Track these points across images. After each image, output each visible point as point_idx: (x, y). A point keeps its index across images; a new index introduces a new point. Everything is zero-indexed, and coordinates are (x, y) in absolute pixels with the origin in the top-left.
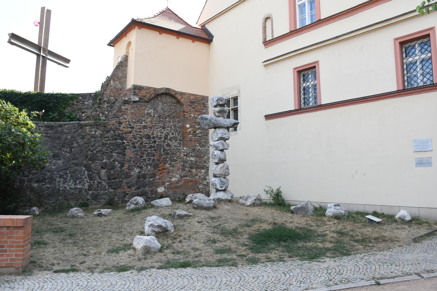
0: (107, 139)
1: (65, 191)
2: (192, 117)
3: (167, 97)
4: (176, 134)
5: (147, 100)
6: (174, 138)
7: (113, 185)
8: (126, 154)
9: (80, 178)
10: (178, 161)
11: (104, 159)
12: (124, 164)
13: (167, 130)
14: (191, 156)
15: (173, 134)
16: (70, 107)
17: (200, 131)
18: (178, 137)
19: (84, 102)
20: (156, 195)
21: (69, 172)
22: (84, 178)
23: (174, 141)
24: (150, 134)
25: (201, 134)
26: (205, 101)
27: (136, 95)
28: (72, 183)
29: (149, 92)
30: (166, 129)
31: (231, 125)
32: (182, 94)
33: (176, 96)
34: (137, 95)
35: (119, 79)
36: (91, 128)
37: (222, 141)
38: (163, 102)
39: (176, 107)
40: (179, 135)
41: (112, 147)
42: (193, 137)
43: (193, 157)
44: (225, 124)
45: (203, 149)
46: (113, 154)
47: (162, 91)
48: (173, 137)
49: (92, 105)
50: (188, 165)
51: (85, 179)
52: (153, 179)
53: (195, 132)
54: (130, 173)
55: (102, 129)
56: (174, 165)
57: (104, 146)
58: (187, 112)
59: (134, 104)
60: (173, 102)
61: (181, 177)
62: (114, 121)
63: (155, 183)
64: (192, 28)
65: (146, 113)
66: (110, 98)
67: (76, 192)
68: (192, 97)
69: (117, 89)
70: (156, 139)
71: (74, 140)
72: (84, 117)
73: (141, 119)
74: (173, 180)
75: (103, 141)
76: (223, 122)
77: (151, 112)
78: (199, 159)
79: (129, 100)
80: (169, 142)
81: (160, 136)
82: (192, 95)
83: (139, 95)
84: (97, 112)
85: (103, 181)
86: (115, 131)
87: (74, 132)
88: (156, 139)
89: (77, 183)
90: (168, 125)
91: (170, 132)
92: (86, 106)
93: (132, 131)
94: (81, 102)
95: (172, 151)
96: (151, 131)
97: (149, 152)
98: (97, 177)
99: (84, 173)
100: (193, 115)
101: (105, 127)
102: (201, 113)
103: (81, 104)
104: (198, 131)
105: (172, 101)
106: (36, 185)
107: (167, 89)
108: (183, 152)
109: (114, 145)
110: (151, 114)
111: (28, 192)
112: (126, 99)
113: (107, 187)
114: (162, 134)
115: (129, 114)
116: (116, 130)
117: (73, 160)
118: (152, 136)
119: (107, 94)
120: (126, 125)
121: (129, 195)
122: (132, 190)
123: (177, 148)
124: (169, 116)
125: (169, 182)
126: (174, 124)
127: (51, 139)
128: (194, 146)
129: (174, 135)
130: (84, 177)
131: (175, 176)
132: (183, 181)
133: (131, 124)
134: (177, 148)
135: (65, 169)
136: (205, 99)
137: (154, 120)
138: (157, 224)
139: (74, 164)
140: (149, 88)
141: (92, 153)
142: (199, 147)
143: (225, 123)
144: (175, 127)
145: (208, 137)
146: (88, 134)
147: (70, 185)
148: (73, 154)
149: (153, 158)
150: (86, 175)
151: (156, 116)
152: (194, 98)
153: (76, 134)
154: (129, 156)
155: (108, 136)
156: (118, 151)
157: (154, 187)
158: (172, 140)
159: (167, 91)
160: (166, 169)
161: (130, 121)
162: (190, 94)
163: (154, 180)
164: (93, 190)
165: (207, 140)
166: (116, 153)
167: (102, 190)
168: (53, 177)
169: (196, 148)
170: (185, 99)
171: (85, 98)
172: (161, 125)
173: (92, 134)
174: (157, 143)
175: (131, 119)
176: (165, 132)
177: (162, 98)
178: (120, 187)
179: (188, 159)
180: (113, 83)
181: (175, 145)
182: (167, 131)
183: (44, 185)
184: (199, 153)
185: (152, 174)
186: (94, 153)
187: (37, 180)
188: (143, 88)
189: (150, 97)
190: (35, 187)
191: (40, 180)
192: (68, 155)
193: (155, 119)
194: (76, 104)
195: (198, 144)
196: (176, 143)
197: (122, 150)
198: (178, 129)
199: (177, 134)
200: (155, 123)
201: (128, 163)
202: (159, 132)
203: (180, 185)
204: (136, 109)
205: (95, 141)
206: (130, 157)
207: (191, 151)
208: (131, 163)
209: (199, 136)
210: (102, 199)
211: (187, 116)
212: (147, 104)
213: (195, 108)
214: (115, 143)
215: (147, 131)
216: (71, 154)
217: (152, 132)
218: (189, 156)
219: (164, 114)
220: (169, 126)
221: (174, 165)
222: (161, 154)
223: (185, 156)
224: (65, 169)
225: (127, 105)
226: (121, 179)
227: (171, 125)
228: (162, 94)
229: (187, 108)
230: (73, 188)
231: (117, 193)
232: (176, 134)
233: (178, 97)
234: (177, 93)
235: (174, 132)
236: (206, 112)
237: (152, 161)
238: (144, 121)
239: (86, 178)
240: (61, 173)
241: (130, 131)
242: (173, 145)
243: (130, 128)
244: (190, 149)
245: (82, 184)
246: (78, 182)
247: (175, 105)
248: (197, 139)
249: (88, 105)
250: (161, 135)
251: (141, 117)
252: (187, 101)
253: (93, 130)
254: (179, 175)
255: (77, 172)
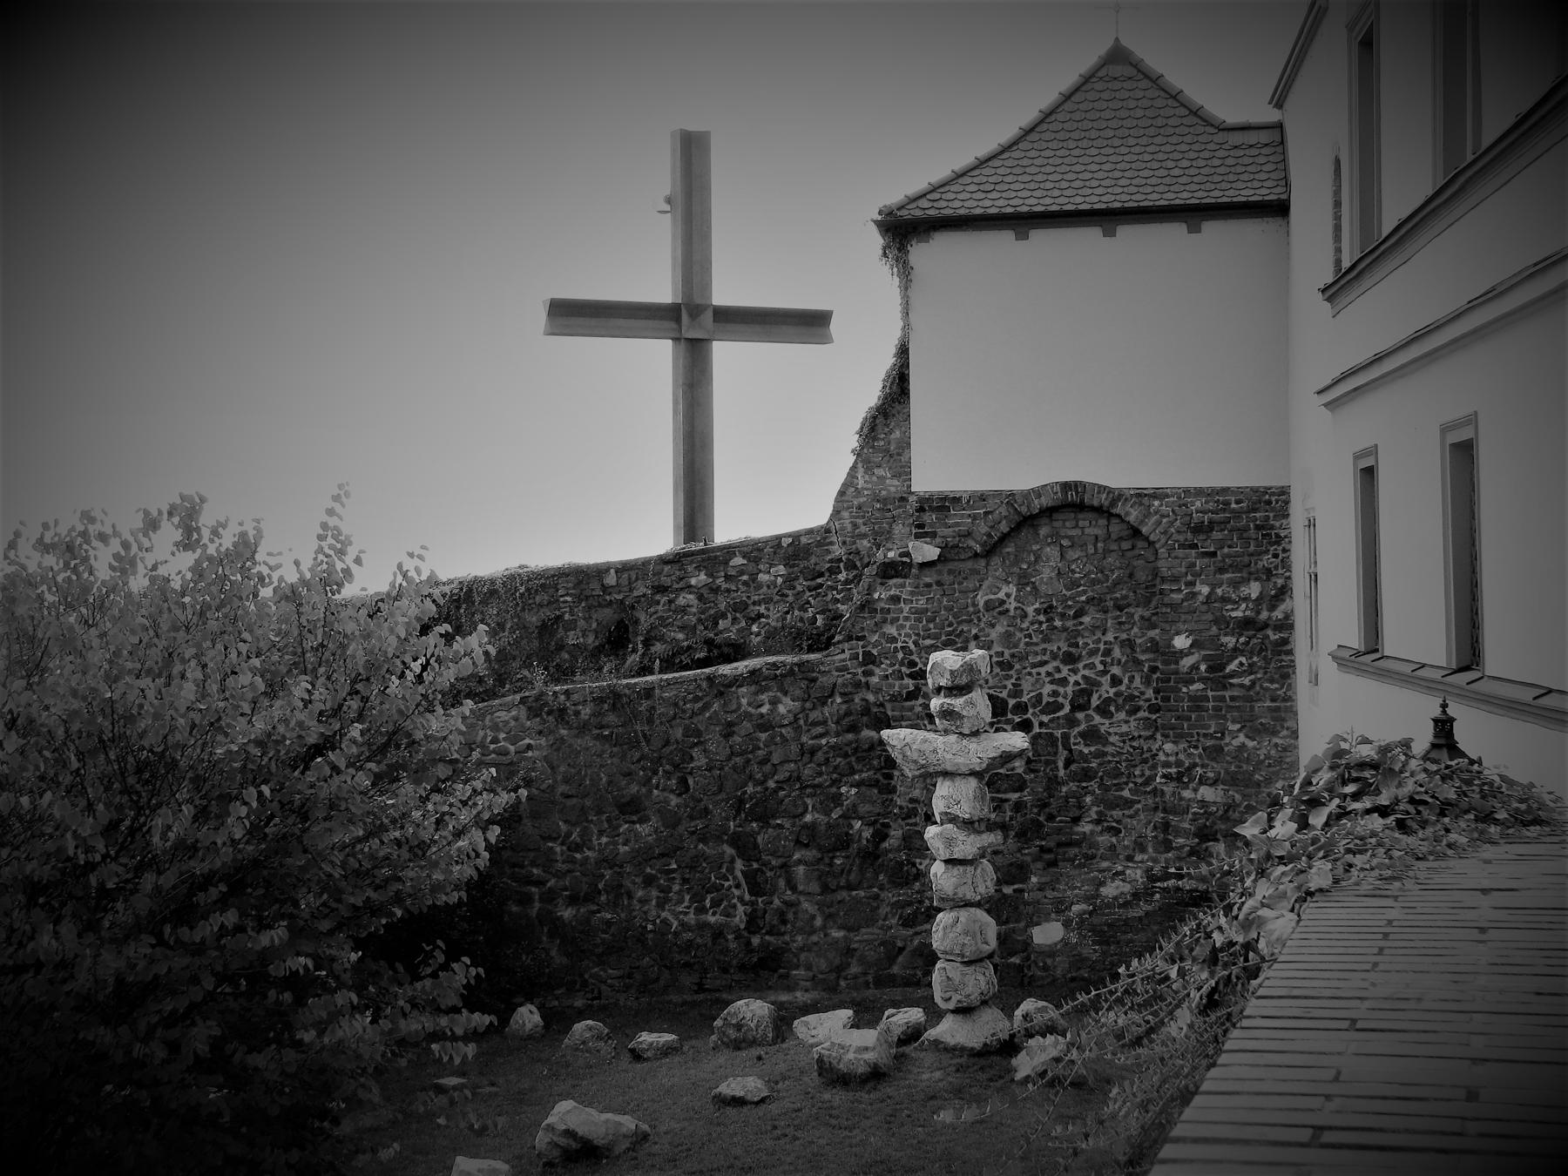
0: (820, 730)
1: (663, 934)
2: (1201, 598)
3: (1081, 516)
4: (1132, 679)
5: (978, 549)
6: (1120, 701)
7: (842, 914)
8: (895, 787)
9: (717, 888)
10: (1139, 806)
11: (806, 811)
12: (887, 826)
13: (1085, 667)
14: (1201, 783)
15: (1116, 681)
16: (265, 867)
17: (1243, 660)
18: (1143, 693)
19: (753, 577)
20: (1028, 958)
21: (675, 866)
22: (730, 887)
23: (1122, 715)
24: (1004, 695)
25: (1253, 677)
26: (1273, 510)
27: (925, 535)
28: (688, 908)
29: (986, 513)
30: (1080, 665)
31: (984, 766)
32: (1141, 496)
33: (1118, 510)
34: (933, 535)
35: (891, 456)
36: (756, 693)
37: (950, 826)
38: (1061, 545)
39: (1129, 554)
40: (1147, 681)
41: (839, 760)
42: (1210, 694)
43: (1211, 785)
44: (957, 764)
45: (1262, 748)
46: (844, 790)
47: (1045, 501)
48: (1116, 694)
49: (784, 582)
50: (1186, 825)
51: (733, 890)
52: (1016, 886)
53: (1222, 667)
54: (914, 865)
55: (798, 692)
56: (1118, 822)
57: (806, 758)
58: (1176, 580)
59: (927, 571)
60: (1114, 536)
61: (1152, 878)
62: (847, 655)
63: (1027, 904)
64: (1237, 138)
65: (981, 604)
66: (854, 543)
67: (699, 940)
68: (1198, 504)
69: (884, 501)
70: (1029, 715)
71: (696, 744)
72: (758, 634)
73: (962, 631)
74: (1110, 890)
75: (804, 739)
76: (948, 756)
77: (1008, 595)
78: (1244, 796)
79: (904, 559)
80: (1097, 719)
81: (1051, 700)
82: (1199, 492)
83: (940, 534)
84: (806, 611)
85: (802, 899)
86: (851, 693)
87: (694, 714)
88: (1033, 714)
89: (705, 906)
90: (1092, 646)
91: (1105, 672)
92: (765, 588)
93: (918, 689)
94: (745, 578)
95: (1110, 762)
96: (1008, 677)
97: (997, 774)
98: (782, 883)
99: (731, 870)
100: (1205, 590)
101: (814, 680)
102: (1250, 573)
103: (745, 583)
104: (1236, 662)
105: (1109, 534)
106: (567, 913)
107: (1066, 486)
108: (1167, 765)
109: (847, 752)
110: (1006, 606)
111: (545, 938)
112: (891, 555)
113: (818, 922)
114: (1061, 690)
115: (906, 619)
116: (853, 690)
117: (692, 818)
118: (1012, 702)
119: (843, 529)
120: (892, 665)
121: (905, 953)
122: (917, 934)
123: (1135, 744)
124: (1096, 602)
125: (1088, 899)
126: (1124, 636)
127: (615, 746)
128: (1215, 732)
129: (1123, 688)
130: (731, 883)
131: (1123, 873)
132: (1157, 896)
133: (917, 660)
134: (1135, 744)
135: (662, 855)
136: (1269, 502)
137: (1022, 630)
138: (564, 1127)
139: (694, 837)
140: (983, 497)
141: (759, 789)
142: (1242, 738)
143: (960, 760)
144: (1129, 651)
145: (1290, 685)
146: (748, 715)
147: (679, 914)
148: (692, 797)
149: (1017, 795)
150: (739, 874)
151: (1030, 610)
152: (1211, 506)
153: (701, 717)
154: (906, 794)
155: (821, 719)
156: (864, 775)
157: (1017, 921)
158: (1112, 709)
159: (1072, 496)
160: (1078, 844)
161: (912, 647)
162: (1187, 491)
163: (1021, 891)
164: (764, 931)
165: (1285, 700)
166: (852, 786)
167: (801, 931)
168: (622, 885)
169: (1227, 745)
170: (1163, 516)
171: (757, 561)
172: (1055, 649)
173: (762, 715)
174: (1036, 730)
175: (914, 638)
176: (1078, 678)
177: (1056, 524)
178: (871, 921)
179: (1187, 794)
180: (867, 477)
181: (1127, 734)
182: (1087, 672)
183: (594, 912)
184: (1245, 767)
185: (1011, 864)
186: (767, 789)
187: (570, 897)
188: (956, 500)
189: (989, 535)
190: (567, 922)
191: (582, 894)
192: (673, 803)
193: (1024, 626)
194: (724, 586)
195: (1234, 722)
196: (1133, 724)
197: (882, 768)
198: (1143, 657)
199: (1137, 682)
200: (1027, 644)
201: (903, 823)
202: (1048, 679)
203: (1141, 913)
204: (935, 592)
205: (770, 742)
206: (912, 800)
207: (1200, 756)
208: (916, 824)
209: (1242, 686)
210: (797, 967)
211: (1174, 596)
212: (988, 564)
213: (1214, 554)
214: (850, 743)
215: (990, 684)
216: (685, 800)
217: (1013, 684)
218: (1191, 780)
219: (1070, 598)
220: (1099, 649)
221: (1118, 822)
222: (1056, 777)
223: (1173, 784)
224: (662, 855)
225: (895, 581)
226: (875, 890)
227: (1105, 643)
228: (1049, 512)
229: (1176, 557)
230: (693, 922)
231: (855, 946)
232: (1132, 679)
233: (1128, 514)
234: (1117, 496)
235: (1125, 671)
236: (1276, 568)
237: (1012, 811)
238: (976, 637)
239: (738, 886)
240: (648, 870)
241: (912, 688)
242: (1116, 734)
243: (911, 676)
244: (1196, 747)
245: (725, 908)
246: (708, 903)
247: (1126, 545)
248: (1233, 698)
249: (768, 587)
250: (1055, 694)
251: (959, 623)
252: (1171, 523)
253: (764, 697)
254: (1140, 868)
255: (704, 865)
